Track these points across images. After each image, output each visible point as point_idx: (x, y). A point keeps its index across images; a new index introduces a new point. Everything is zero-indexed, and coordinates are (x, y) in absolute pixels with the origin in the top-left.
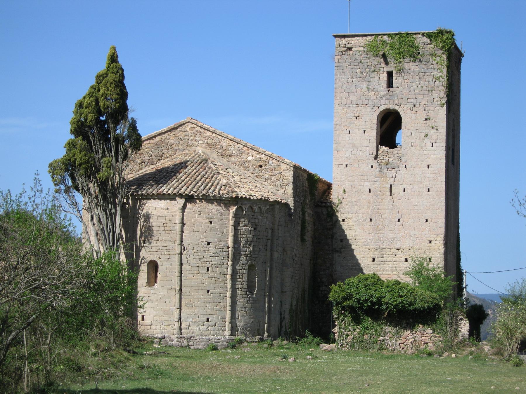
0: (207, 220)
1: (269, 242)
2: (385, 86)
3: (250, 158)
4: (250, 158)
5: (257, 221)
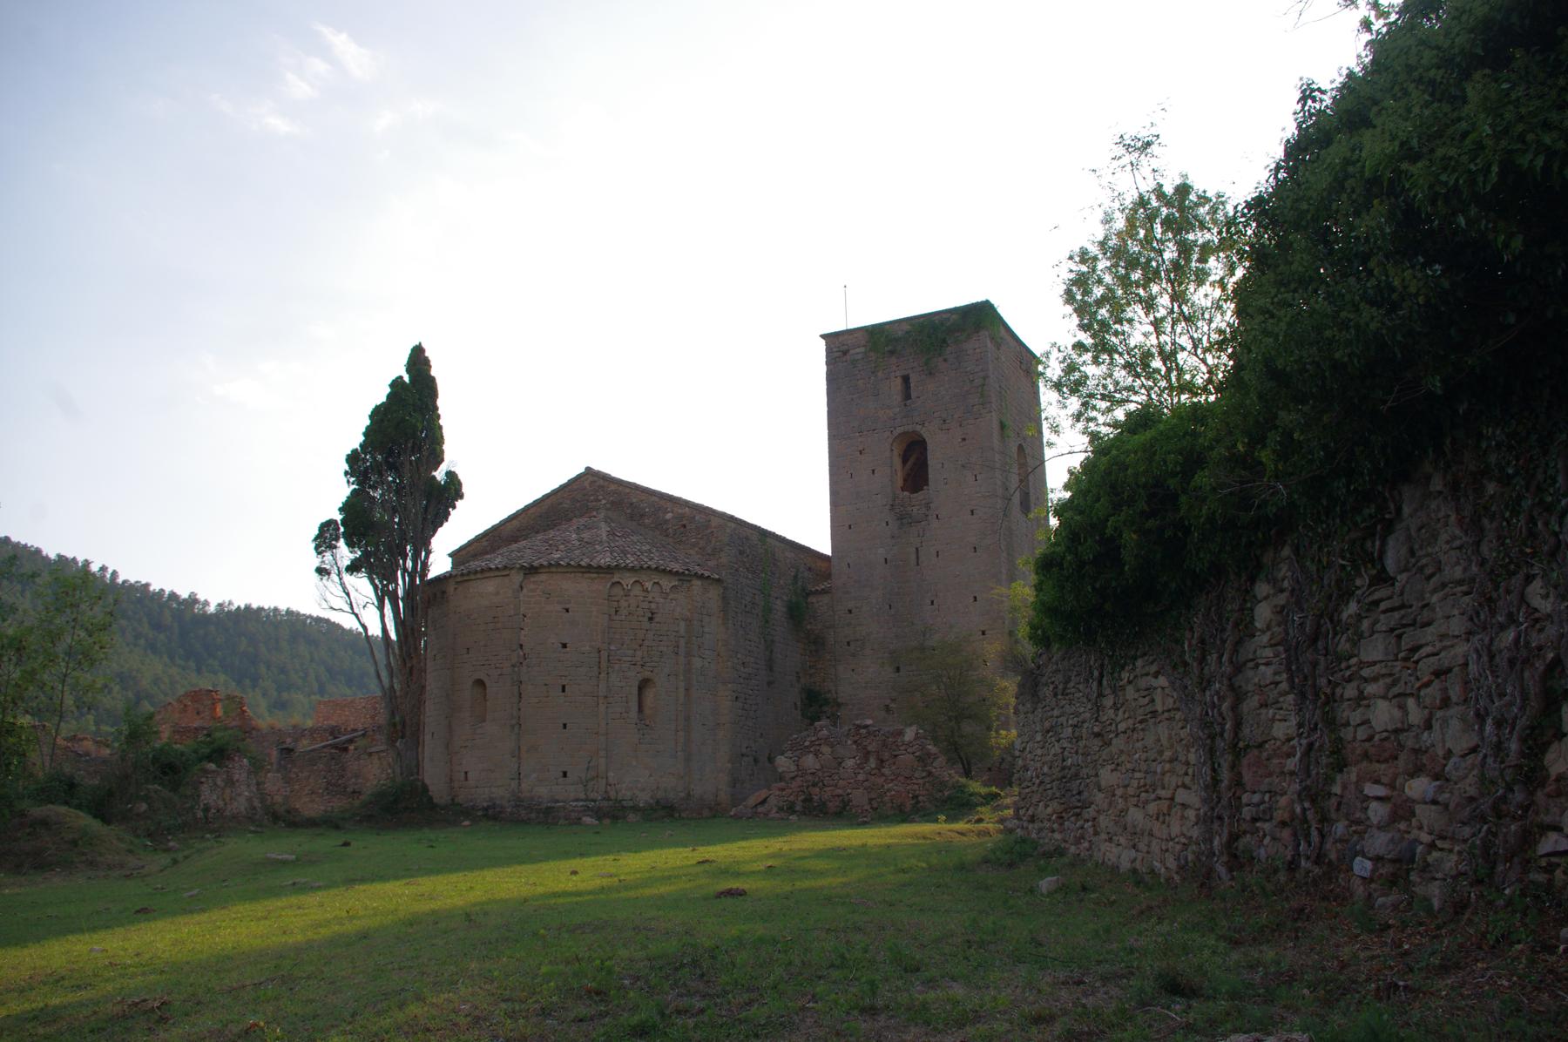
0: (559, 608)
1: (682, 642)
2: (899, 398)
3: (669, 516)
4: (669, 516)
5: (653, 606)
